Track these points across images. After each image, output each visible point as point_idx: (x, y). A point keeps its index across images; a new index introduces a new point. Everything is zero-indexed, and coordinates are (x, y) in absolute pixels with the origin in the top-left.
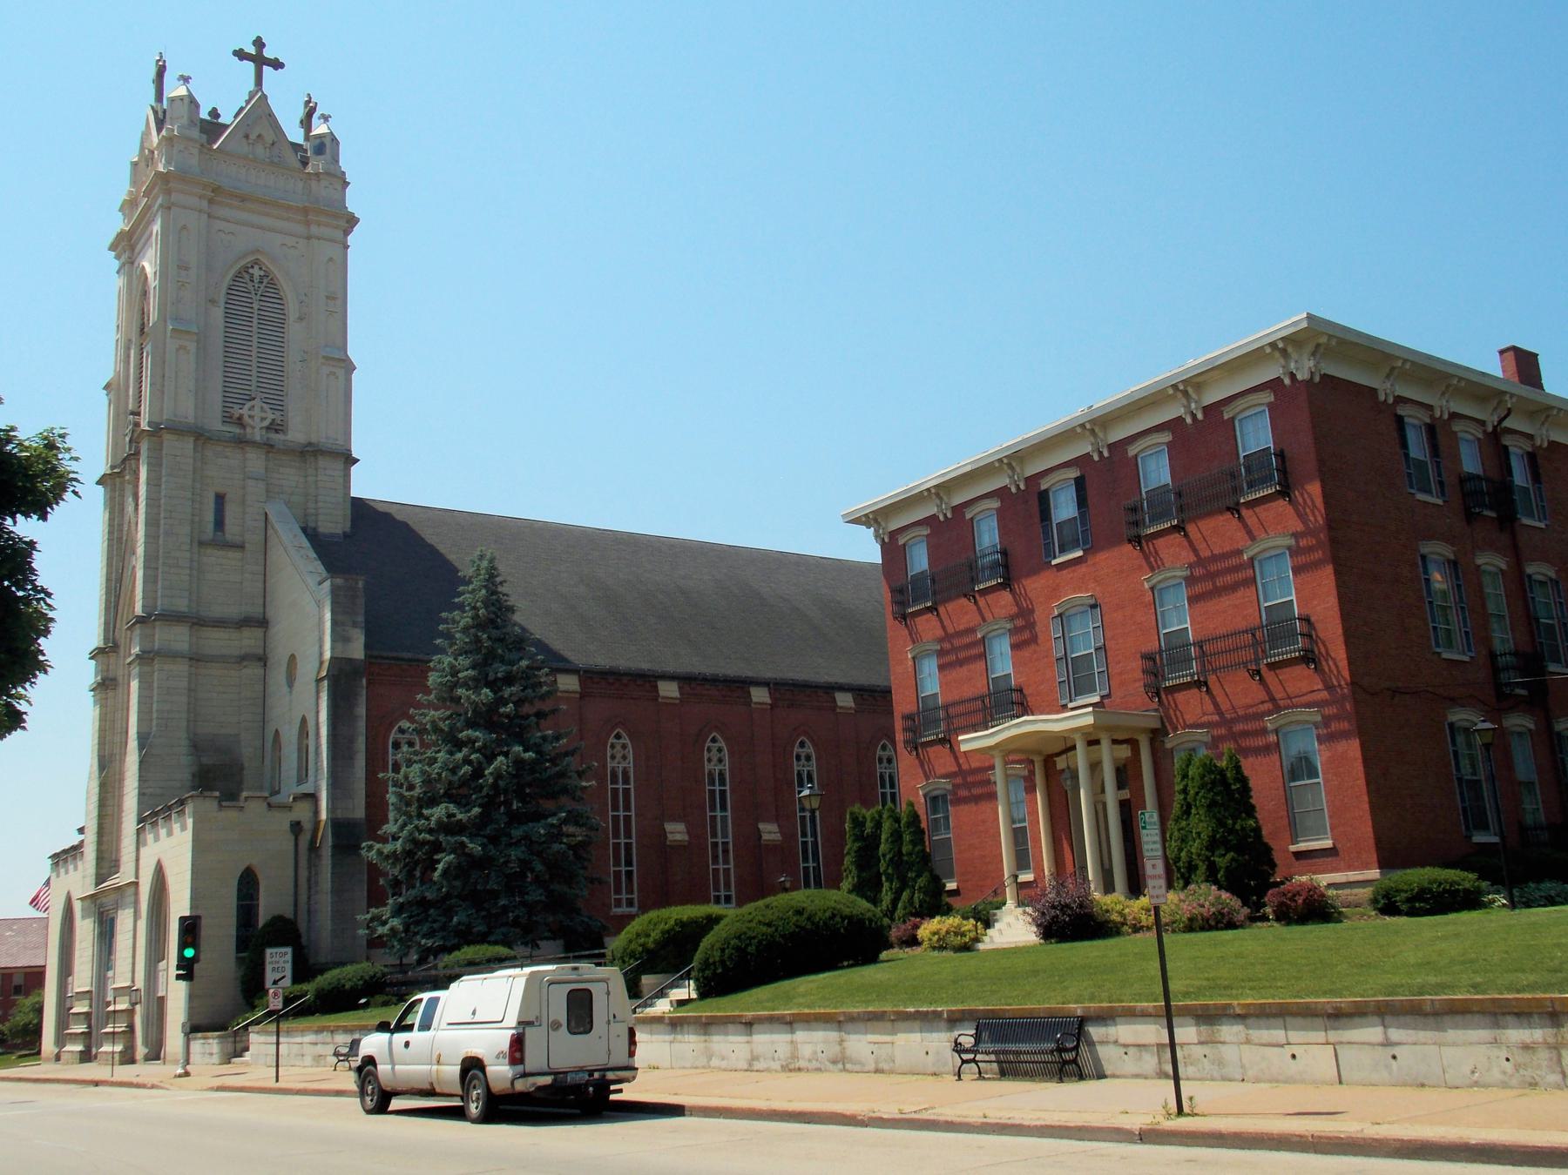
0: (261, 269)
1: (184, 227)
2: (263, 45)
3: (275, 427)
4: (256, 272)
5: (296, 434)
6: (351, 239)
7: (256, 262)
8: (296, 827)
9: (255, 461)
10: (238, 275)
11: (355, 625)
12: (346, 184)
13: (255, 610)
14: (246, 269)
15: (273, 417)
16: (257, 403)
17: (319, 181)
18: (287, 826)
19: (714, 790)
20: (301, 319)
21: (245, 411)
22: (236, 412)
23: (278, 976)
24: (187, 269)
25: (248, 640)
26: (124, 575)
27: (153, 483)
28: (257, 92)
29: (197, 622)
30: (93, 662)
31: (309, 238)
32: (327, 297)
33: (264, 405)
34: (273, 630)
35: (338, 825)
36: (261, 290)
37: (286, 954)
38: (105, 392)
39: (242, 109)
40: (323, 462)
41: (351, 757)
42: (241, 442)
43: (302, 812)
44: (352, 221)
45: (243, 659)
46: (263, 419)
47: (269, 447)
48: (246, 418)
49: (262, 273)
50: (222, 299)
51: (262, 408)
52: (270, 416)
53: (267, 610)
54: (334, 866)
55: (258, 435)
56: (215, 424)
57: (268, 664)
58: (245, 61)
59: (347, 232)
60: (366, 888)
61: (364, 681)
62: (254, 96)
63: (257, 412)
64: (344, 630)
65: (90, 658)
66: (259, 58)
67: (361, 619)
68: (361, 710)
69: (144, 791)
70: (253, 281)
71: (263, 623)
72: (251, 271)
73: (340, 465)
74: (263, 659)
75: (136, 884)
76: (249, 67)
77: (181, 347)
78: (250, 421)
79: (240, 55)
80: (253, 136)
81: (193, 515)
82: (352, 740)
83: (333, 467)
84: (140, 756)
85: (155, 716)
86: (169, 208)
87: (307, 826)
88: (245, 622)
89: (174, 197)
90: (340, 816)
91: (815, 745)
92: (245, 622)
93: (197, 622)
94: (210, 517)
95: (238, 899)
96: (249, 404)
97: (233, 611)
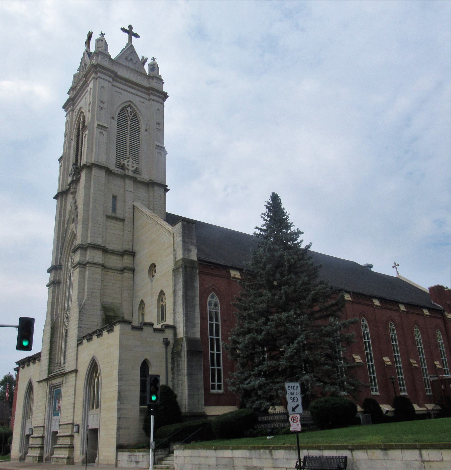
0: (131, 109)
1: (103, 87)
2: (132, 28)
3: (136, 171)
4: (129, 109)
5: (145, 176)
6: (165, 104)
7: (129, 106)
8: (166, 343)
9: (129, 185)
10: (122, 110)
11: (192, 244)
12: (163, 83)
13: (129, 248)
14: (125, 107)
15: (137, 166)
16: (130, 160)
17: (153, 80)
18: (162, 340)
19: (217, 366)
20: (146, 130)
21: (125, 162)
22: (123, 162)
23: (294, 404)
24: (103, 103)
25: (127, 261)
26: (66, 237)
27: (88, 187)
28: (130, 44)
29: (105, 251)
30: (49, 274)
31: (149, 100)
32: (157, 123)
33: (133, 161)
34: (137, 257)
35: (191, 342)
36: (131, 117)
37: (297, 387)
38: (59, 162)
39: (124, 49)
40: (156, 188)
41: (194, 307)
42: (124, 177)
43: (169, 334)
44: (165, 96)
45: (123, 270)
46: (133, 167)
47: (135, 180)
48: (126, 165)
49: (132, 111)
50: (116, 118)
51: (132, 162)
52: (135, 167)
53: (134, 248)
54: (189, 361)
55: (130, 173)
56: (113, 167)
57: (135, 272)
58: (125, 33)
59: (164, 100)
60: (203, 374)
61: (198, 271)
62: (128, 45)
63: (130, 163)
64: (188, 246)
65: (48, 272)
66: (129, 31)
67: (194, 242)
68: (197, 284)
69: (81, 325)
70: (128, 113)
71: (133, 254)
72: (127, 109)
73: (163, 190)
74: (133, 270)
75: (76, 371)
76: (126, 35)
77: (101, 133)
78: (128, 167)
79: (124, 30)
80: (129, 58)
81: (104, 203)
82: (194, 298)
83: (160, 190)
84: (79, 309)
85: (86, 291)
86: (96, 79)
87: (172, 341)
88: (123, 254)
89: (99, 74)
90: (190, 336)
91: (368, 321)
92: (123, 254)
93: (105, 251)
94: (110, 205)
95: (140, 377)
96: (127, 160)
97: (119, 247)
